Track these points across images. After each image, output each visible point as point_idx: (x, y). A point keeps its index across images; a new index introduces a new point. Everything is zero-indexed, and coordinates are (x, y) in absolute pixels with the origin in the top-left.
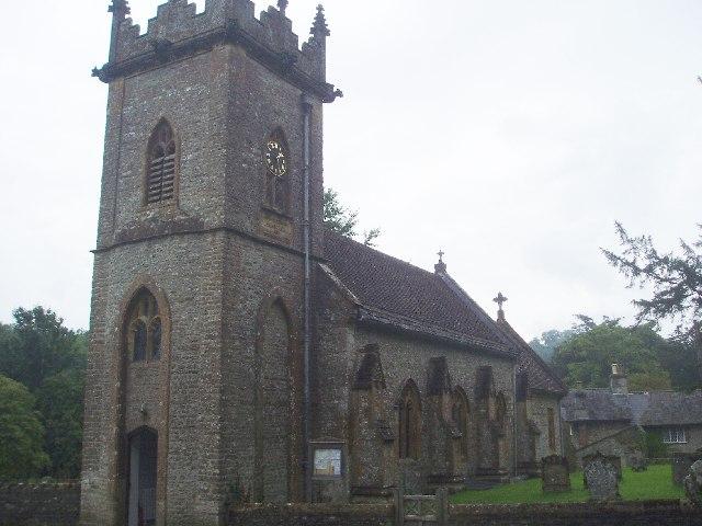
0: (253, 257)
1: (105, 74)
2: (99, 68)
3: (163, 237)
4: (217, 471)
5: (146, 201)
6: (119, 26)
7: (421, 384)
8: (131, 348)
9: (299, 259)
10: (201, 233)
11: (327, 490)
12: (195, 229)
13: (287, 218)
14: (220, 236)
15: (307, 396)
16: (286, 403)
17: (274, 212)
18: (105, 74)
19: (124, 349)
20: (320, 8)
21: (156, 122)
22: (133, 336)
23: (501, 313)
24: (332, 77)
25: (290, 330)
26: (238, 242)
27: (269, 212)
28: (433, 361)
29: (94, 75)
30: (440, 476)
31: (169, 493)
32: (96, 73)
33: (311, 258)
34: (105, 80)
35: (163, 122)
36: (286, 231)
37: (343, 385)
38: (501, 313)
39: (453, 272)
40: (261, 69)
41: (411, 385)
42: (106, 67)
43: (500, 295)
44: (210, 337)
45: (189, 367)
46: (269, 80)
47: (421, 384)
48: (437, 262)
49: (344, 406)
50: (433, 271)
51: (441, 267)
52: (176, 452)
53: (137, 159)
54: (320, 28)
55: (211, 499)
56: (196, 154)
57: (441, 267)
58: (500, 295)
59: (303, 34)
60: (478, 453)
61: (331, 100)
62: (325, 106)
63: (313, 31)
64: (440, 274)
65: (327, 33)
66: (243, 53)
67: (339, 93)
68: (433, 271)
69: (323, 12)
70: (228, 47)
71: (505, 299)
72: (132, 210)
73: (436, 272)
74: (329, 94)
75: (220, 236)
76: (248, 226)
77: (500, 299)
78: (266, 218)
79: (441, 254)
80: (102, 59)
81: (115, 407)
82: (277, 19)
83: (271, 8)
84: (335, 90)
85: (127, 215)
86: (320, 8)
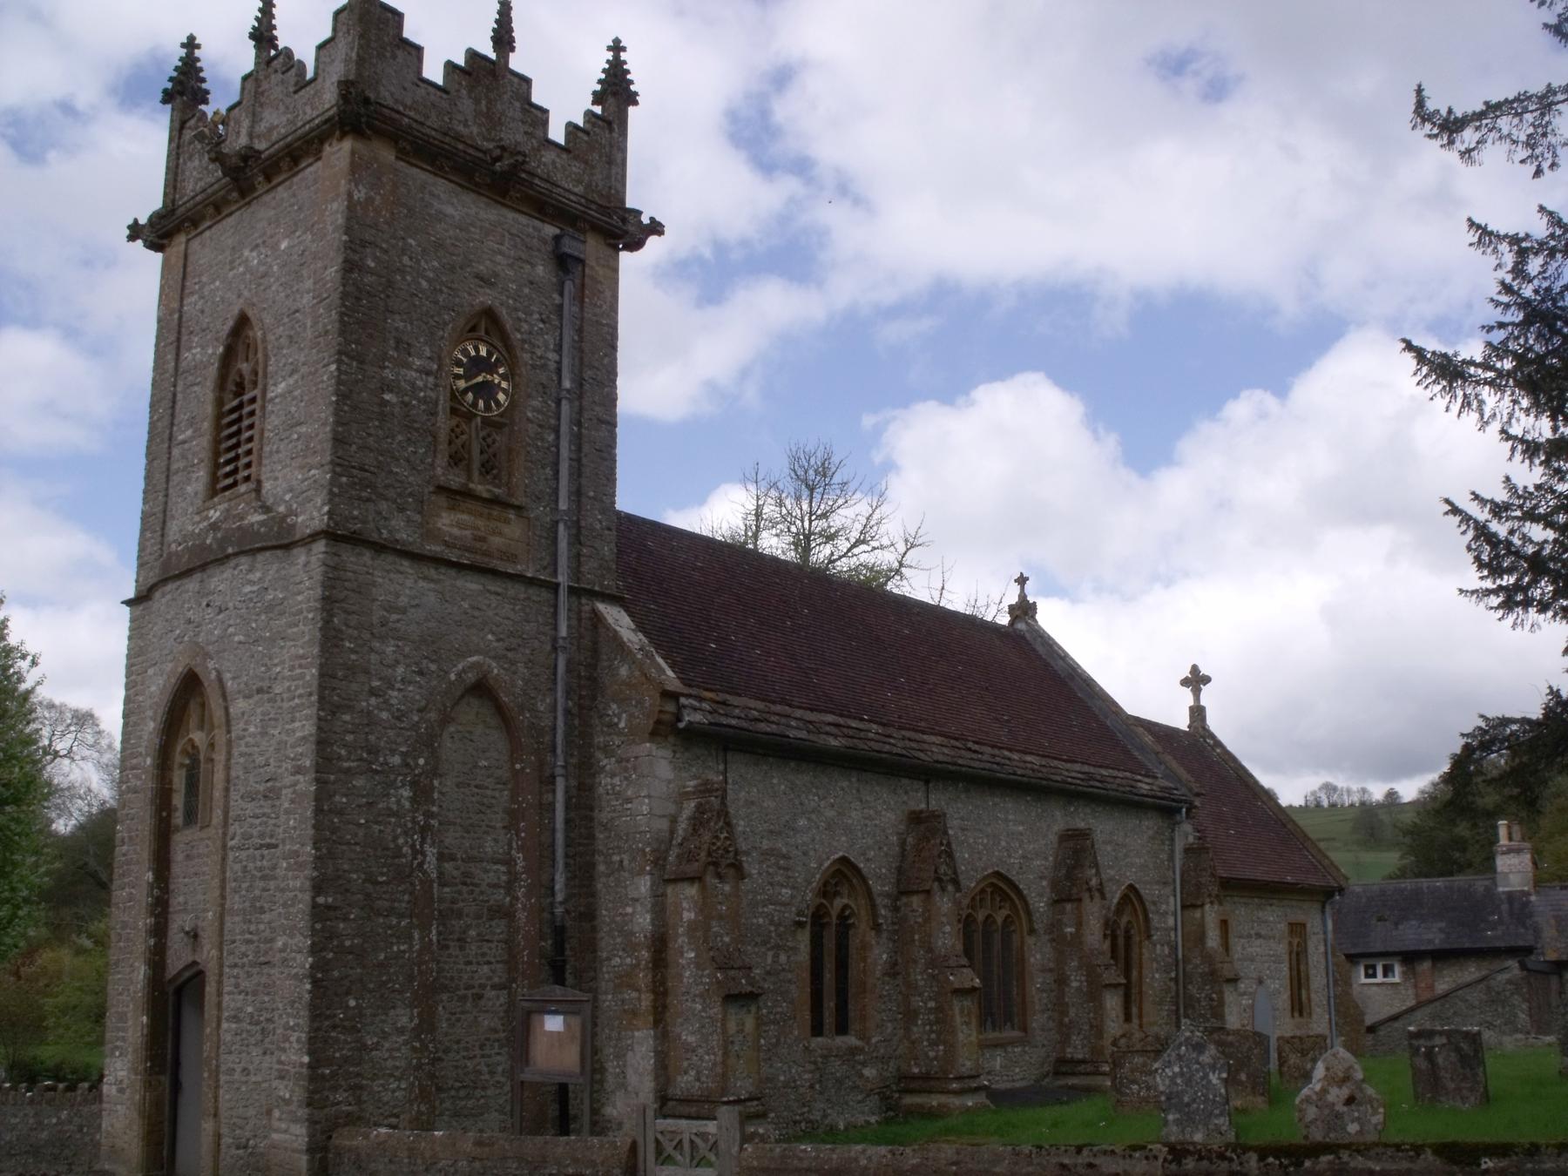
0: (401, 587)
1: (157, 233)
2: (143, 221)
3: (223, 560)
4: (306, 1059)
5: (213, 491)
6: (182, 127)
7: (878, 870)
8: (178, 800)
9: (545, 595)
10: (287, 547)
11: (614, 1107)
12: (282, 542)
13: (506, 505)
14: (320, 546)
15: (559, 897)
16: (508, 914)
17: (466, 494)
18: (157, 233)
19: (163, 797)
20: (617, 47)
21: (230, 323)
22: (183, 772)
23: (1198, 713)
24: (639, 196)
25: (515, 751)
26: (358, 561)
27: (458, 496)
28: (915, 818)
29: (132, 237)
30: (926, 1077)
31: (223, 1106)
32: (135, 232)
33: (572, 591)
34: (154, 246)
35: (243, 322)
36: (512, 531)
37: (641, 872)
38: (1198, 713)
39: (1053, 620)
40: (441, 186)
41: (845, 873)
42: (157, 218)
43: (1195, 669)
44: (298, 770)
45: (262, 835)
46: (456, 207)
47: (878, 870)
48: (1014, 600)
49: (643, 921)
50: (1004, 620)
51: (1023, 610)
52: (235, 1019)
53: (200, 400)
54: (616, 89)
55: (296, 1121)
56: (291, 381)
57: (1023, 610)
58: (1195, 669)
59: (565, 101)
60: (1061, 1023)
61: (635, 245)
62: (625, 257)
63: (598, 98)
64: (1021, 626)
65: (632, 99)
66: (387, 154)
67: (656, 228)
68: (1004, 620)
69: (623, 56)
70: (347, 145)
71: (1207, 680)
72: (192, 519)
73: (1012, 623)
74: (631, 231)
75: (320, 546)
76: (401, 530)
77: (1196, 680)
78: (452, 508)
79: (1022, 581)
80: (149, 200)
81: (144, 922)
82: (489, 77)
83: (472, 55)
84: (645, 220)
85: (187, 523)
86: (617, 47)
